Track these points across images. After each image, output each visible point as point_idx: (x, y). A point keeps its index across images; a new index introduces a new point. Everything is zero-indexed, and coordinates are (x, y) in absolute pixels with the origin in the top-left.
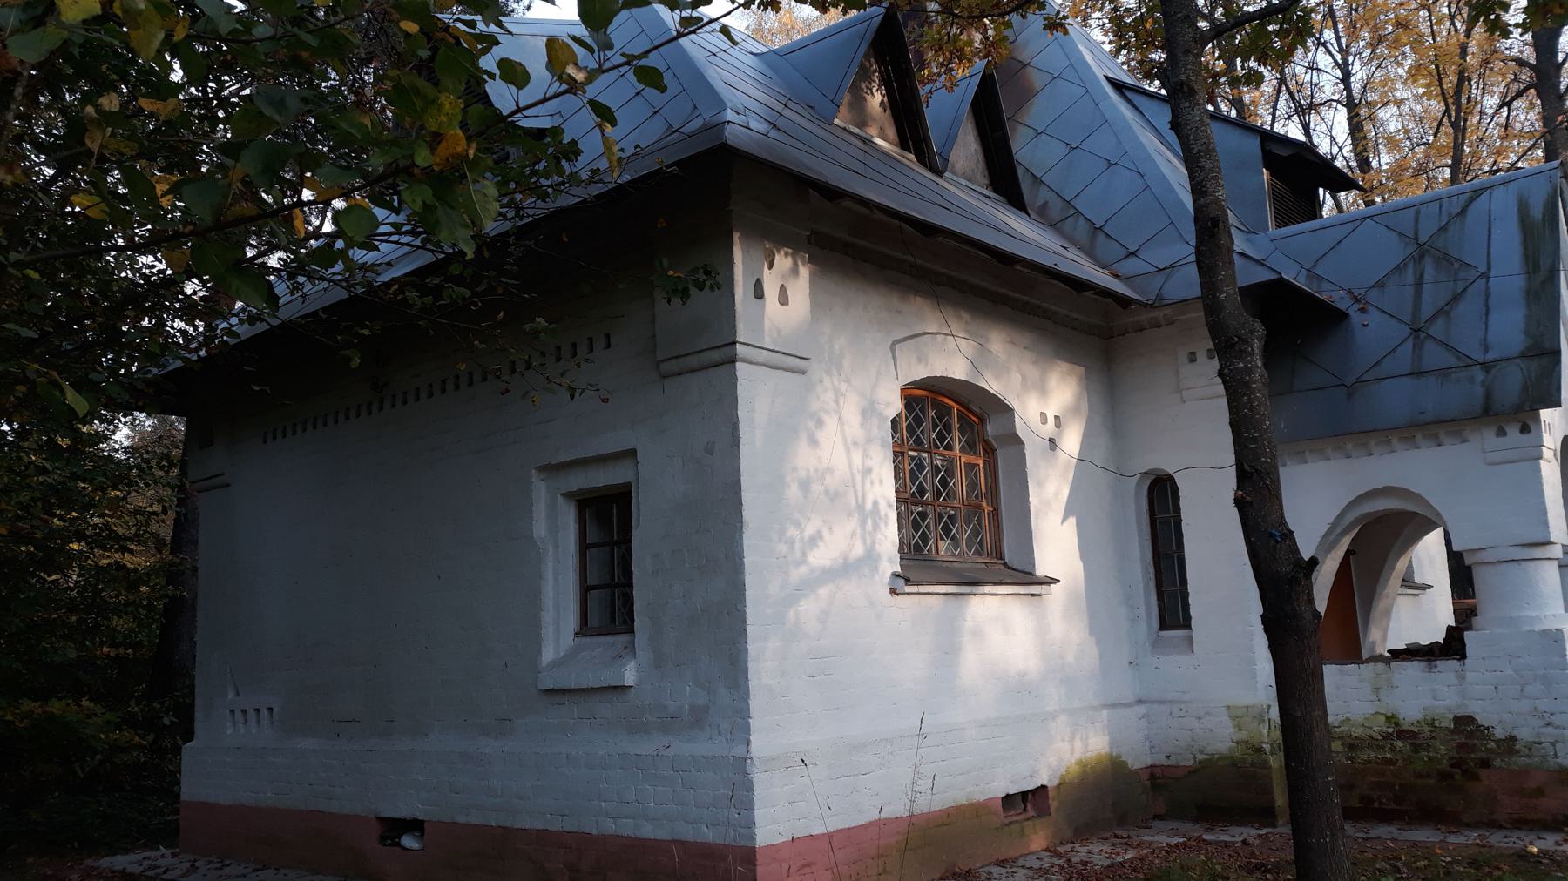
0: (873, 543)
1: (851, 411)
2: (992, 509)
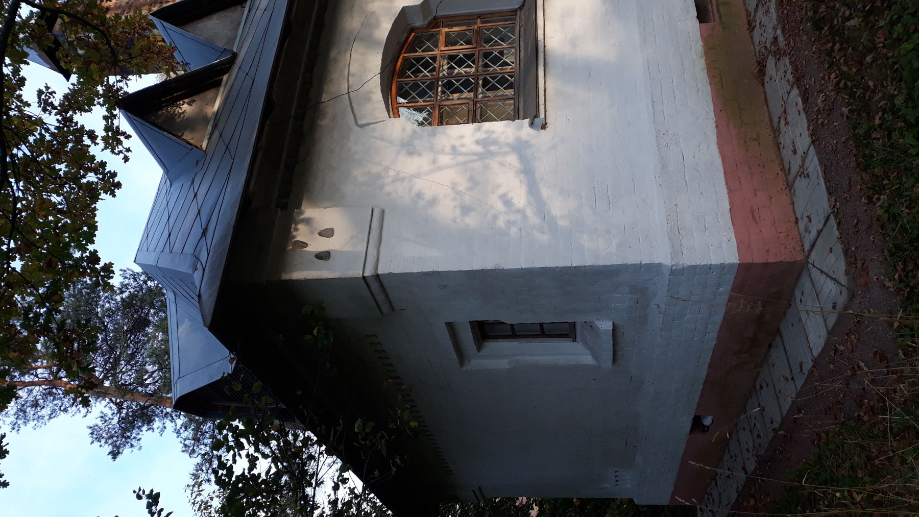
0: (508, 145)
1: (410, 165)
2: (479, 20)
